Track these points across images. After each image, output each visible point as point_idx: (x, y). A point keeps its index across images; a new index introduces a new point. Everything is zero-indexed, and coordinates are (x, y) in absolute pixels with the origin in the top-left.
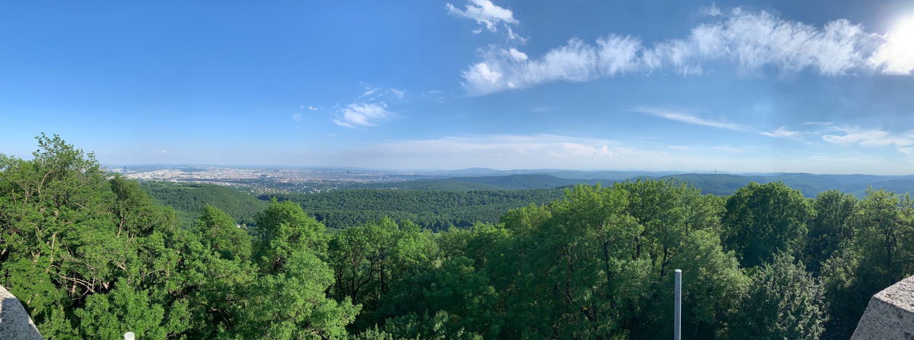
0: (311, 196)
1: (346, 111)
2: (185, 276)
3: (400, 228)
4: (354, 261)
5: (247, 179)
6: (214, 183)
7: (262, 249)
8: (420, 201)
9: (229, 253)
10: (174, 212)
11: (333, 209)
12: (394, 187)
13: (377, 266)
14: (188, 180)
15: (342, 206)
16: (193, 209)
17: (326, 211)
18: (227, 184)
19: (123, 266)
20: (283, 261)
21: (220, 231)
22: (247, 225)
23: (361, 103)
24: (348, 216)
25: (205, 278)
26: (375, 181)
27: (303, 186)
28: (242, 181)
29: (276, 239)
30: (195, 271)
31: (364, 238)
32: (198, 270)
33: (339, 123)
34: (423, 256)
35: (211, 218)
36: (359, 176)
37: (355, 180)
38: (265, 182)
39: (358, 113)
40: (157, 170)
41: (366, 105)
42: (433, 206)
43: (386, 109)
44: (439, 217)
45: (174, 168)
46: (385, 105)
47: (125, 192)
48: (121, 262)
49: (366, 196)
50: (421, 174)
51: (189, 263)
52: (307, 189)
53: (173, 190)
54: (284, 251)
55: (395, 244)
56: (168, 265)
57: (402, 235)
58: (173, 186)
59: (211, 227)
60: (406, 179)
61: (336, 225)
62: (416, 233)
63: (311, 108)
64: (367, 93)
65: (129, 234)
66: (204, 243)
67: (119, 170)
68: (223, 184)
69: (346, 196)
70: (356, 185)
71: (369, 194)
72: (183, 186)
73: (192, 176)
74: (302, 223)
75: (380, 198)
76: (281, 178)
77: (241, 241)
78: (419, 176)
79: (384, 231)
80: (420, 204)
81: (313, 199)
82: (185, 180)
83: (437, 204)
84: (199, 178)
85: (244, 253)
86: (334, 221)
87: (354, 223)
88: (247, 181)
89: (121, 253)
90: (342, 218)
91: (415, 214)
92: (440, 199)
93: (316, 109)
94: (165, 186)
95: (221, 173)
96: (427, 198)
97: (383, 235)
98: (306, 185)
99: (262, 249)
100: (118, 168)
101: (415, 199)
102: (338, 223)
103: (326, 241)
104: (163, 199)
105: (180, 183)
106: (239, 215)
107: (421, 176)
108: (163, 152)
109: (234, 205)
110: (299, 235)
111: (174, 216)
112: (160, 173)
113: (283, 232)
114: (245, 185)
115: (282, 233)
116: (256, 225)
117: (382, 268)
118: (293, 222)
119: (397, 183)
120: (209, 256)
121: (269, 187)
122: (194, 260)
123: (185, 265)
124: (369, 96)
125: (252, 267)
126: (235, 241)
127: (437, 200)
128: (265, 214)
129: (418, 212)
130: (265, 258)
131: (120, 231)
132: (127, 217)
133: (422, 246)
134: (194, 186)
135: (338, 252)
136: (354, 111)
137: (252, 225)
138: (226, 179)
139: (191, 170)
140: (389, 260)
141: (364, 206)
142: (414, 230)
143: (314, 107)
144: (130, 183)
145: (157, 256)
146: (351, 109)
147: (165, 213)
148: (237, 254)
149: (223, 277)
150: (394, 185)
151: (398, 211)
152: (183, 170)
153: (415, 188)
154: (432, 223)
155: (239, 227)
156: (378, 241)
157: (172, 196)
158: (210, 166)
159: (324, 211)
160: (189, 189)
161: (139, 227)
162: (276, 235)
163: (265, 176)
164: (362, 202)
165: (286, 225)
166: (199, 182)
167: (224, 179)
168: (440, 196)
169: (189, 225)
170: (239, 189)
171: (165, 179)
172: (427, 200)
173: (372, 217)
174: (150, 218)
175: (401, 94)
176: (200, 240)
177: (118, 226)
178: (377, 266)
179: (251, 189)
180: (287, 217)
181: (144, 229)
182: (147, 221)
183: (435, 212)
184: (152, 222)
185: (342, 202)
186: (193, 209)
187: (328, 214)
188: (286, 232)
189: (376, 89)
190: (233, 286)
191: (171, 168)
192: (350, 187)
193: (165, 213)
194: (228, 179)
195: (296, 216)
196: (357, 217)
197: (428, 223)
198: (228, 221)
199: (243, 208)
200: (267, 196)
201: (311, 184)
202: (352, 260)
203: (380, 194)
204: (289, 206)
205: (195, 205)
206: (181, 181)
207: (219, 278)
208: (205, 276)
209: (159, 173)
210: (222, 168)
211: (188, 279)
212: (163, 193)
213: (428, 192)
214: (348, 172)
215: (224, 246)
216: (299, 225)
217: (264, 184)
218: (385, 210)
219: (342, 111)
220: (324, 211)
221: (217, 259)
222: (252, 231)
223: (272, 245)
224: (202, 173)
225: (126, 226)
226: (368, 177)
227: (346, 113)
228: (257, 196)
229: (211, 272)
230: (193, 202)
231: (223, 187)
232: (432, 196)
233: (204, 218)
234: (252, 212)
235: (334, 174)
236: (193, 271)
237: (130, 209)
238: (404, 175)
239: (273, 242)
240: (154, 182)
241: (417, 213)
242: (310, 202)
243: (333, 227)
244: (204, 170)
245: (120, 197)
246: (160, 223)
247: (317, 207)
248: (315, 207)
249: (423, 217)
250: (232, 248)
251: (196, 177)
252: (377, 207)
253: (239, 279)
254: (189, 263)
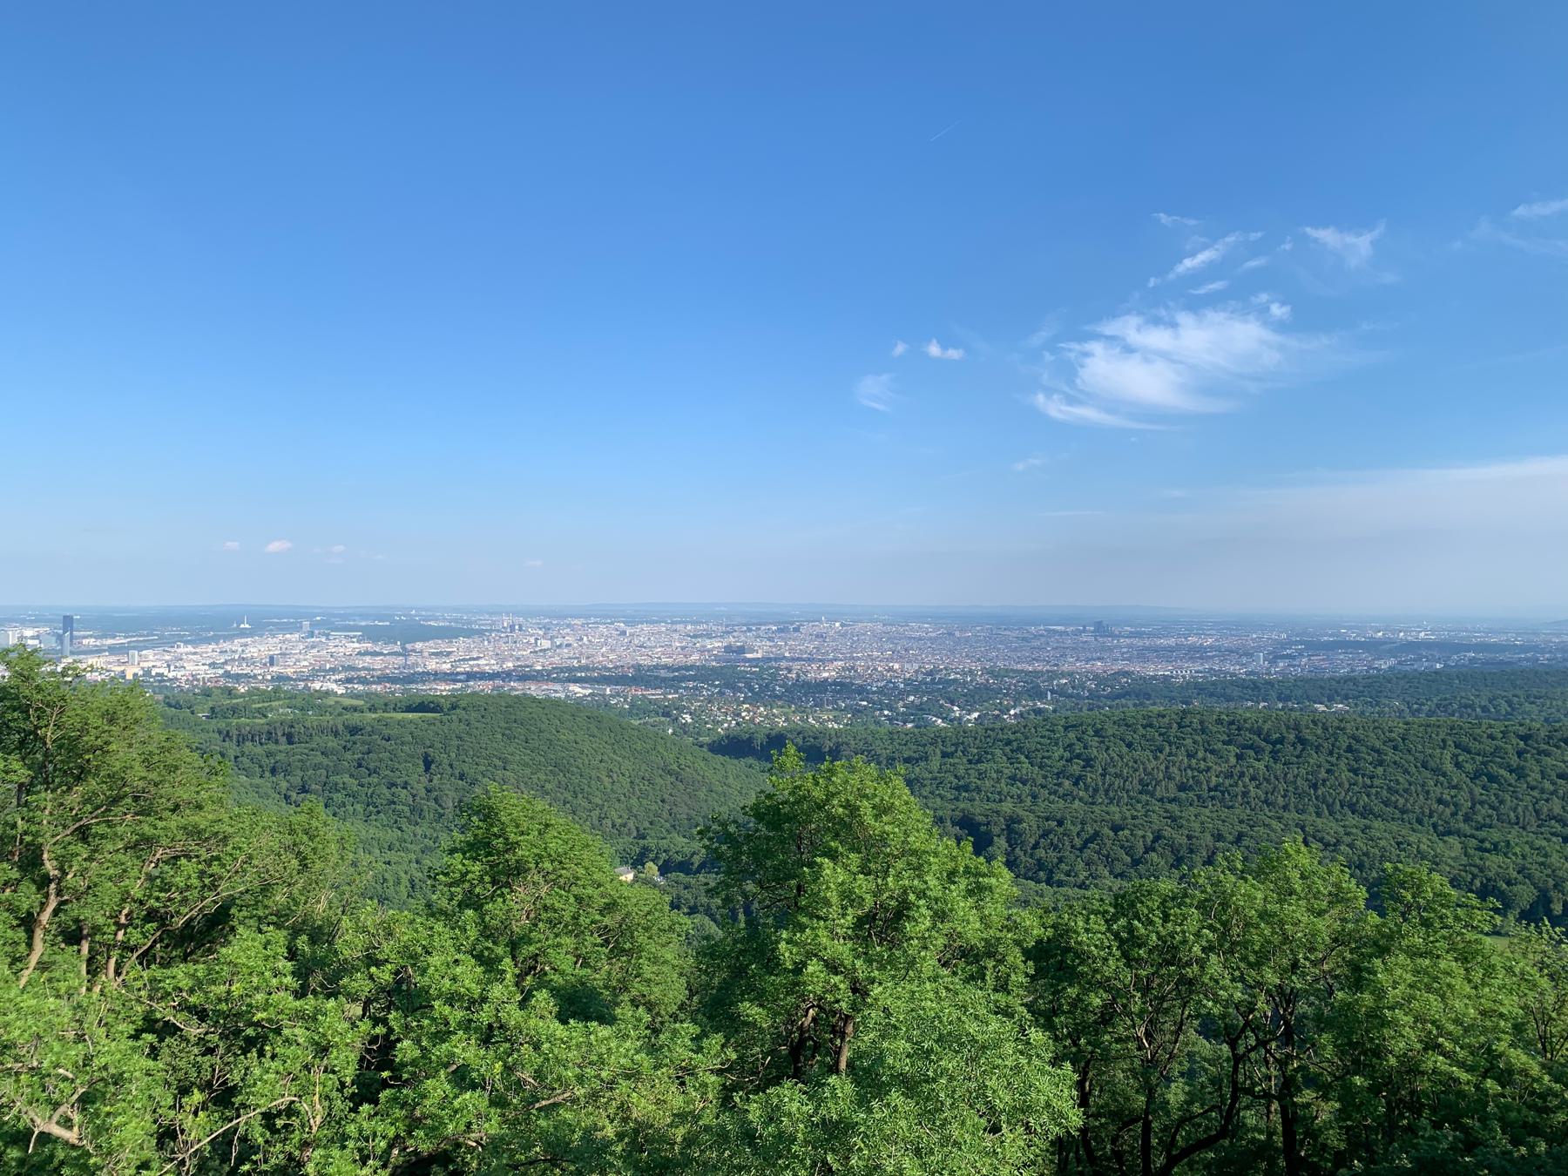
0: (938, 738)
1: (1087, 354)
2: (398, 1113)
3: (1375, 903)
4: (1148, 1035)
5: (666, 667)
6: (517, 689)
7: (739, 972)
8: (1475, 777)
9: (593, 994)
11: (1035, 797)
13: (1265, 1075)
14: (393, 680)
15: (1076, 784)
17: (1007, 807)
18: (578, 690)
19: (67, 1123)
20: (834, 1024)
21: (548, 902)
22: (664, 870)
23: (1163, 312)
24: (1107, 831)
25: (494, 1112)
26: (1238, 669)
27: (903, 694)
28: (643, 677)
29: (802, 928)
30: (448, 1087)
32: (462, 1078)
33: (1056, 409)
34: (1519, 1057)
35: (511, 847)
36: (1156, 650)
37: (1136, 668)
38: (742, 676)
39: (1149, 355)
40: (243, 634)
41: (1184, 318)
43: (1281, 327)
45: (328, 624)
46: (1277, 310)
47: (70, 746)
48: (56, 1105)
49: (1188, 742)
50: (1478, 638)
51: (417, 1053)
52: (920, 708)
54: (836, 979)
55: (1358, 977)
56: (318, 1076)
57: (1390, 937)
58: (322, 710)
59: (508, 885)
60: (1392, 661)
61: (1051, 872)
62: (1471, 936)
63: (934, 350)
64: (1188, 263)
65: (90, 961)
66: (489, 963)
67: (29, 633)
68: (557, 691)
69: (1094, 742)
70: (1142, 690)
71: (1203, 731)
72: (373, 709)
73: (412, 659)
74: (914, 860)
75: (1258, 751)
76: (810, 660)
77: (641, 938)
78: (1468, 648)
79: (1296, 911)
80: (1478, 790)
81: (945, 755)
82: (381, 680)
84: (446, 667)
85: (656, 993)
86: (1041, 853)
87: (1136, 863)
88: (663, 673)
89: (60, 1058)
90: (1078, 842)
91: (1450, 839)
93: (954, 354)
94: (281, 712)
95: (546, 644)
98: (915, 691)
99: (739, 972)
100: (24, 623)
101: (1449, 767)
102: (1061, 860)
103: (1018, 943)
104: (273, 771)
105: (357, 696)
106: (631, 824)
107: (1479, 647)
108: (275, 546)
109: (607, 780)
110: (902, 911)
111: (333, 847)
112: (259, 648)
113: (833, 896)
114: (655, 694)
115: (827, 903)
116: (702, 866)
117: (1288, 1087)
118: (874, 856)
120: (513, 1015)
121: (755, 699)
122: (442, 1036)
123: (403, 1065)
124: (1198, 277)
125: (699, 1050)
126: (619, 942)
130: (751, 1010)
131: (39, 947)
132: (82, 873)
133: (1510, 1005)
134: (422, 707)
135: (1072, 992)
136: (1129, 350)
137: (684, 867)
138: (571, 669)
139: (407, 632)
140: (1329, 1052)
141: (1182, 788)
142: (1457, 918)
143: (944, 347)
144: (100, 701)
145: (250, 1043)
146: (1111, 339)
147: (288, 839)
148: (625, 997)
149: (575, 1101)
150: (1333, 689)
151: (1352, 820)
152: (370, 634)
153: (1443, 707)
154: (1553, 894)
155: (630, 877)
157: (320, 759)
158: (500, 614)
159: (993, 806)
161: (151, 915)
162: (800, 909)
163: (741, 650)
164: (1174, 770)
165: (845, 867)
166: (443, 689)
167: (562, 670)
169: (398, 882)
170: (630, 712)
171: (281, 678)
172: (1520, 773)
173: (1219, 837)
174: (215, 868)
175: (1357, 246)
176: (467, 945)
177: (28, 923)
178: (1265, 1075)
179: (681, 709)
180: (846, 828)
181: (179, 922)
182: (195, 882)
184: (223, 885)
185: (1076, 768)
186: (417, 811)
187: (1013, 821)
188: (848, 897)
189: (1231, 239)
190: (620, 1136)
191: (314, 625)
192: (1107, 697)
193: (288, 839)
194: (581, 669)
195: (887, 828)
196: (1150, 837)
197: (1525, 894)
198: (586, 854)
199: (644, 795)
200: (750, 740)
201: (936, 689)
202: (1141, 1032)
204: (855, 780)
205: (429, 791)
206: (361, 687)
207: (555, 1105)
208: (492, 1103)
209: (253, 651)
210: (552, 620)
211: (414, 1123)
212: (272, 747)
213: (1522, 731)
214: (1101, 629)
215: (566, 963)
216: (900, 865)
217: (735, 689)
218: (1285, 808)
219: (1072, 355)
220: (993, 806)
221: (542, 1019)
222: (686, 894)
224: (459, 647)
225: (77, 921)
226: (1196, 653)
227: (1088, 361)
228: (705, 739)
229: (519, 1084)
230: (419, 781)
231: (556, 703)
232: (1548, 754)
233: (476, 848)
234: (683, 812)
235: (1036, 643)
236: (438, 1087)
237: (102, 829)
238: (1380, 643)
240: (230, 692)
241: (1458, 833)
242: (935, 763)
243: (1038, 882)
244: (469, 633)
245: (42, 776)
246: (266, 889)
247: (966, 788)
248: (957, 788)
250: (602, 974)
251: (432, 665)
252: (1245, 794)
253: (642, 1107)
254: (417, 1053)
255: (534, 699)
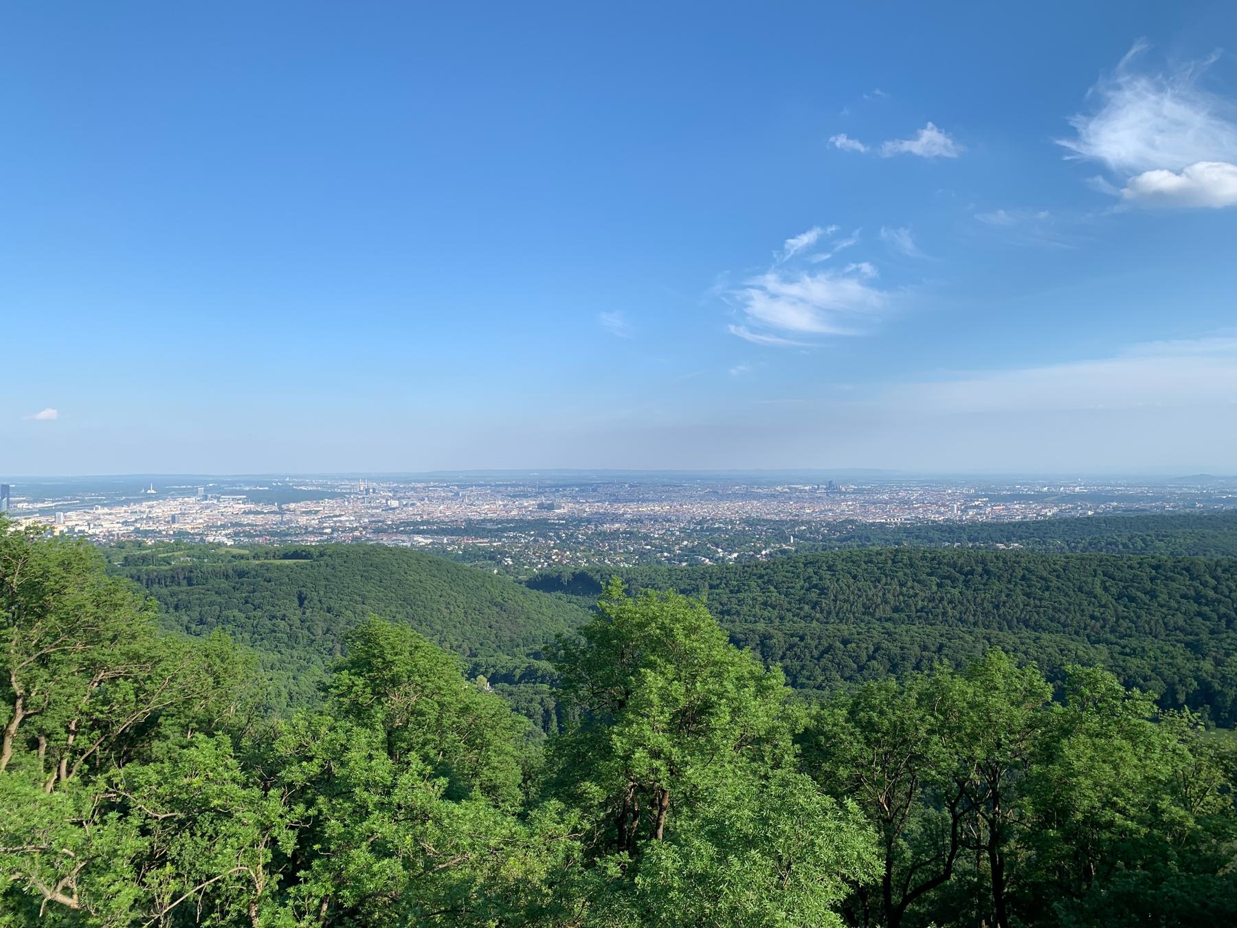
0: (706, 574)
5: (491, 520)
8: (1118, 598)
10: (241, 652)
11: (782, 618)
12: (1009, 540)
16: (293, 637)
18: (421, 540)
27: (678, 541)
28: (473, 528)
29: (630, 723)
31: (921, 722)
32: (381, 850)
35: (388, 665)
40: (149, 498)
42: (1180, 620)
43: (871, 283)
44: (1207, 665)
45: (219, 489)
49: (900, 574)
53: (215, 574)
54: (657, 763)
55: (1049, 753)
60: (1055, 510)
62: (1134, 721)
68: (405, 542)
69: (827, 575)
70: (864, 533)
71: (912, 566)
72: (256, 557)
73: (287, 517)
78: (1112, 499)
80: (1121, 608)
81: (711, 587)
83: (1199, 614)
88: (489, 526)
92: (1211, 593)
94: (182, 559)
96: (1148, 586)
97: (994, 716)
101: (1098, 590)
104: (176, 608)
105: (243, 547)
107: (1120, 498)
109: (445, 612)
110: (706, 708)
112: (163, 509)
113: (655, 698)
114: (483, 543)
115: (650, 704)
119: (1021, 524)
127: (1198, 598)
128: (583, 640)
129: (1112, 638)
134: (296, 555)
136: (774, 296)
138: (415, 523)
139: (283, 495)
141: (896, 610)
142: (1125, 708)
144: (56, 553)
151: (1025, 633)
152: (253, 497)
156: (974, 737)
160: (278, 567)
161: (96, 724)
164: (889, 596)
166: (312, 540)
167: (408, 524)
168: (1213, 582)
171: (181, 534)
172: (1153, 595)
173: (925, 648)
179: (504, 554)
183: (1187, 645)
185: (813, 595)
192: (837, 540)
194: (423, 523)
196: (872, 648)
198: (446, 670)
200: (559, 577)
203: (954, 566)
205: (302, 621)
209: (157, 512)
212: (175, 588)
213: (1154, 562)
218: (975, 624)
223: (619, 744)
224: (326, 506)
230: (295, 615)
231: (404, 551)
233: (360, 665)
237: (58, 656)
239: (620, 734)
240: (140, 545)
241: (1108, 642)
244: (332, 496)
246: (188, 702)
249: (1137, 661)
251: (303, 520)
252: (944, 614)
255: (386, 548)
